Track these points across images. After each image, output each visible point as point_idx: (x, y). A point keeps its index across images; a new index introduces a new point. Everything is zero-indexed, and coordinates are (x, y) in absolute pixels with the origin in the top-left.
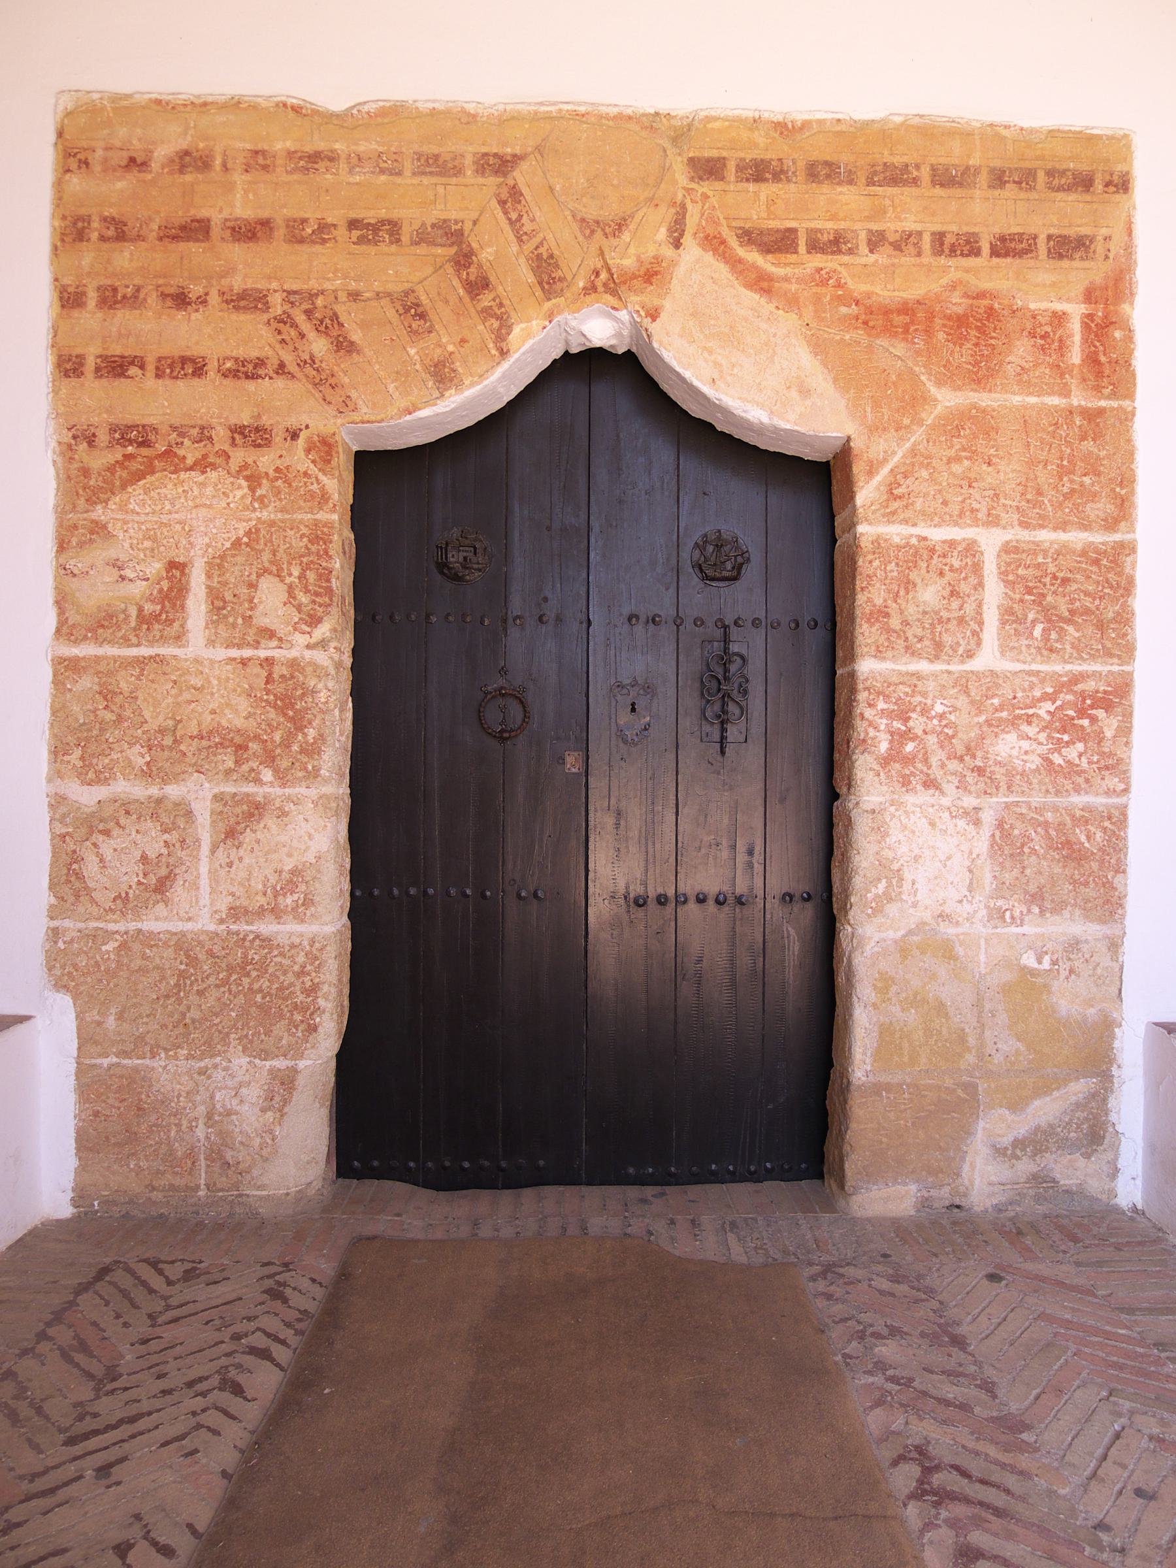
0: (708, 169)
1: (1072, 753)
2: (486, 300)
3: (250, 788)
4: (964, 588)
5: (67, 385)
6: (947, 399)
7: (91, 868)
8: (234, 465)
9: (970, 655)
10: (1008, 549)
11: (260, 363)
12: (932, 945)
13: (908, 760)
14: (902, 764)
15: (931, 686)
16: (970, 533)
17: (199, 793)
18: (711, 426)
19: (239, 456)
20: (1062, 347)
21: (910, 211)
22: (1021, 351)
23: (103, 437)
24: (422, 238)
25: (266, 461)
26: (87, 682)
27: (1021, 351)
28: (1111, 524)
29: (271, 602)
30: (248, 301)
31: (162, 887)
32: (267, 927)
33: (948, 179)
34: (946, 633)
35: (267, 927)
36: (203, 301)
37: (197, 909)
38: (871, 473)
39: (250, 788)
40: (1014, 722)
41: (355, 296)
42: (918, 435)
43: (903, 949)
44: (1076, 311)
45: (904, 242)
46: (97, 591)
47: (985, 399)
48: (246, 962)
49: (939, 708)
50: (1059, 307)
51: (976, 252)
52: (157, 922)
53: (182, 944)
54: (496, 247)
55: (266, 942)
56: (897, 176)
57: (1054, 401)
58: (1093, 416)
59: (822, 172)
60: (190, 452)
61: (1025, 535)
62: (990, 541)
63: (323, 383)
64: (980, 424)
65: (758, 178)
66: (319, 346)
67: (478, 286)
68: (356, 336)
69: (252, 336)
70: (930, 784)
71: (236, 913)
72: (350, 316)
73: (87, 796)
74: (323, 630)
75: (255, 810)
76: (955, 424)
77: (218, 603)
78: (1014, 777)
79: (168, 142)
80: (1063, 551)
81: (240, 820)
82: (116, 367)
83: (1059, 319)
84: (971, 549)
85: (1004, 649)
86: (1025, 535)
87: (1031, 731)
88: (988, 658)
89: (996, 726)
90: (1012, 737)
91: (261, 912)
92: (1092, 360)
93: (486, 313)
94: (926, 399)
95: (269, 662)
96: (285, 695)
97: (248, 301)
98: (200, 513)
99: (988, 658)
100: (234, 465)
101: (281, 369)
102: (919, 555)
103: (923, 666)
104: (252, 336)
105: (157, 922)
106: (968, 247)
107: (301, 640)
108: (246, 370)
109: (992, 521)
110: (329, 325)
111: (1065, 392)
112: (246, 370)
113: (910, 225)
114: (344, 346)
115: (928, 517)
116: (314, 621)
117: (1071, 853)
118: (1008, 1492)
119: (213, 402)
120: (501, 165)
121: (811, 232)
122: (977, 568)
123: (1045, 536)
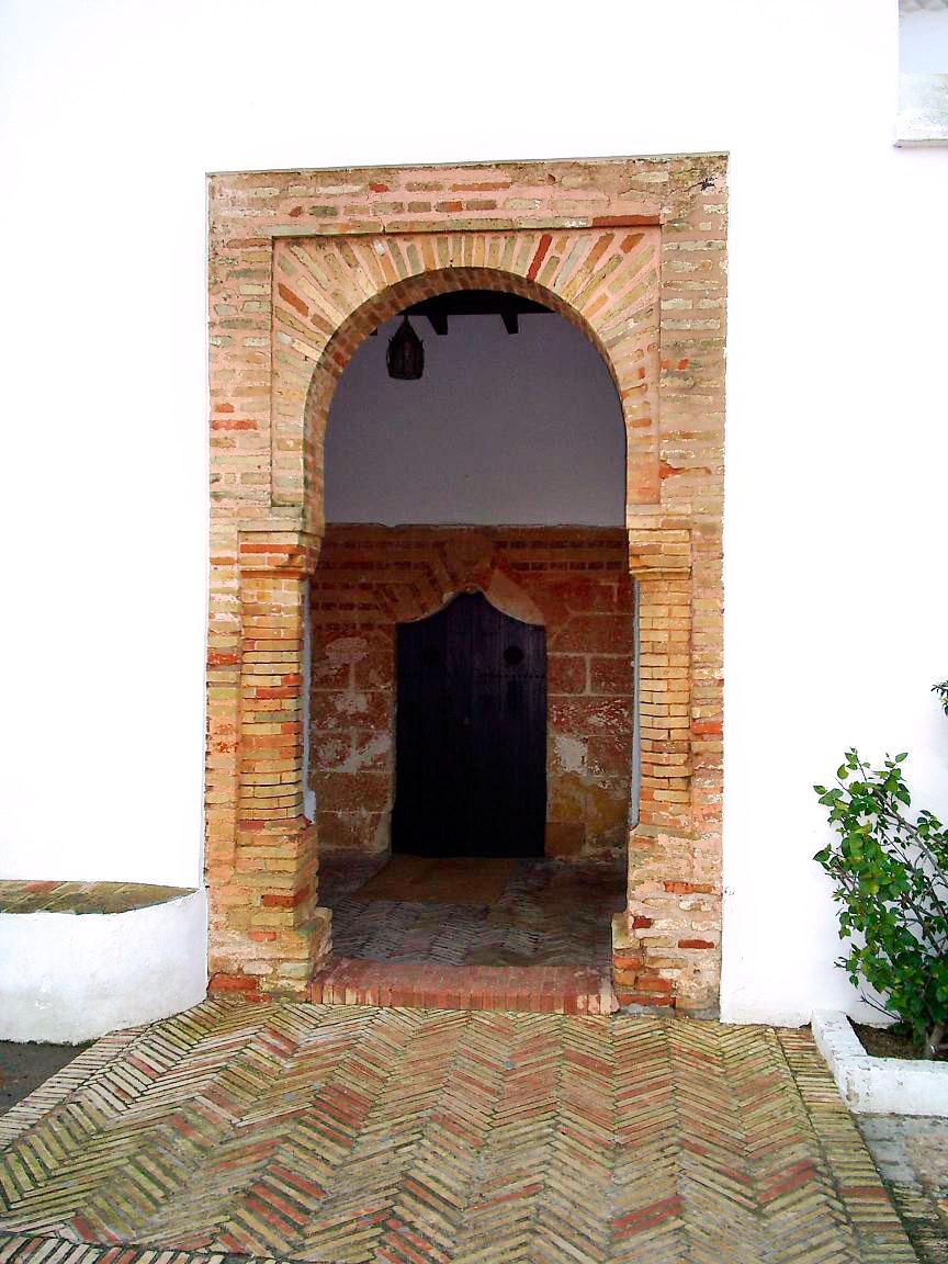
0: (502, 545)
1: (614, 722)
2: (436, 586)
3: (367, 730)
4: (580, 671)
5: (314, 612)
6: (574, 614)
7: (321, 754)
8: (363, 635)
9: (581, 692)
10: (593, 660)
11: (370, 605)
12: (573, 778)
13: (562, 723)
14: (561, 726)
15: (569, 701)
16: (582, 655)
17: (353, 731)
18: (118, 912)
19: (364, 633)
20: (611, 596)
21: (563, 556)
22: (598, 599)
23: (324, 627)
24: (416, 567)
25: (372, 634)
26: (320, 699)
27: (598, 599)
28: (627, 652)
29: (373, 675)
30: (365, 587)
31: (342, 760)
32: (373, 772)
33: (577, 545)
34: (573, 685)
35: (373, 772)
36: (353, 587)
37: (351, 765)
38: (551, 636)
39: (367, 730)
40: (596, 712)
41: (397, 585)
42: (566, 626)
43: (562, 780)
44: (615, 585)
45: (561, 566)
46: (324, 671)
47: (588, 614)
48: (366, 782)
49: (572, 708)
50: (609, 584)
51: (583, 568)
52: (340, 769)
53: (346, 775)
54: (440, 571)
55: (373, 776)
56: (560, 545)
57: (609, 614)
58: (621, 619)
59: (537, 545)
60: (350, 631)
61: (600, 655)
62: (588, 657)
63: (389, 612)
64: (586, 621)
65: (518, 547)
66: (387, 600)
67: (433, 582)
68: (398, 597)
69: (368, 598)
70: (570, 731)
71: (363, 768)
72: (396, 592)
73: (320, 734)
74: (389, 684)
75: (369, 737)
76: (576, 620)
77: (358, 676)
78: (596, 729)
79: (658, 159)
80: (611, 660)
81: (365, 740)
82: (328, 606)
83: (610, 587)
84: (582, 659)
85: (592, 690)
86: (600, 655)
87: (601, 715)
88: (588, 692)
89: (590, 714)
90: (595, 717)
91: (371, 767)
92: (620, 601)
93: (436, 590)
94: (567, 613)
95: (373, 693)
96: (377, 703)
97: (365, 587)
98: (350, 650)
99: (588, 692)
100: (363, 635)
101: (377, 608)
102: (566, 662)
103: (566, 695)
104: (368, 598)
105: (340, 769)
106: (582, 566)
107: (383, 687)
108: (365, 607)
109: (590, 651)
110: (390, 594)
111: (611, 611)
112: (365, 607)
113: (564, 560)
114: (394, 600)
115: (569, 650)
116: (386, 681)
117: (613, 752)
118: (170, 1032)
119: (356, 616)
120: (439, 545)
121: (532, 564)
122: (584, 665)
123: (605, 655)
